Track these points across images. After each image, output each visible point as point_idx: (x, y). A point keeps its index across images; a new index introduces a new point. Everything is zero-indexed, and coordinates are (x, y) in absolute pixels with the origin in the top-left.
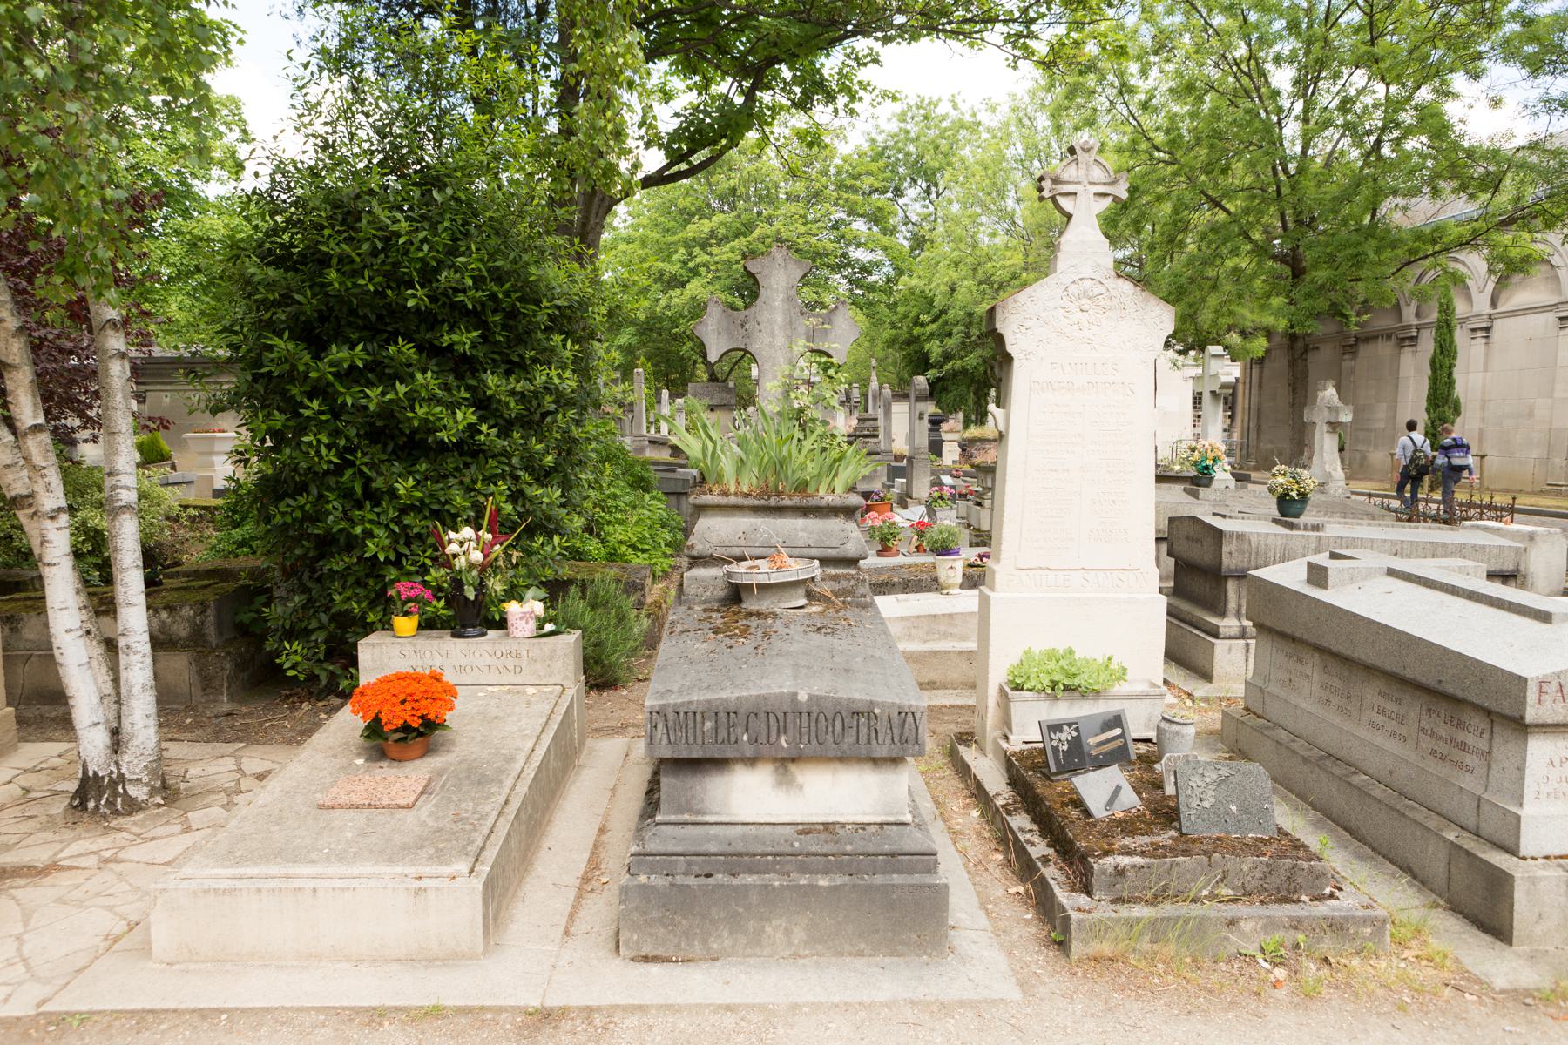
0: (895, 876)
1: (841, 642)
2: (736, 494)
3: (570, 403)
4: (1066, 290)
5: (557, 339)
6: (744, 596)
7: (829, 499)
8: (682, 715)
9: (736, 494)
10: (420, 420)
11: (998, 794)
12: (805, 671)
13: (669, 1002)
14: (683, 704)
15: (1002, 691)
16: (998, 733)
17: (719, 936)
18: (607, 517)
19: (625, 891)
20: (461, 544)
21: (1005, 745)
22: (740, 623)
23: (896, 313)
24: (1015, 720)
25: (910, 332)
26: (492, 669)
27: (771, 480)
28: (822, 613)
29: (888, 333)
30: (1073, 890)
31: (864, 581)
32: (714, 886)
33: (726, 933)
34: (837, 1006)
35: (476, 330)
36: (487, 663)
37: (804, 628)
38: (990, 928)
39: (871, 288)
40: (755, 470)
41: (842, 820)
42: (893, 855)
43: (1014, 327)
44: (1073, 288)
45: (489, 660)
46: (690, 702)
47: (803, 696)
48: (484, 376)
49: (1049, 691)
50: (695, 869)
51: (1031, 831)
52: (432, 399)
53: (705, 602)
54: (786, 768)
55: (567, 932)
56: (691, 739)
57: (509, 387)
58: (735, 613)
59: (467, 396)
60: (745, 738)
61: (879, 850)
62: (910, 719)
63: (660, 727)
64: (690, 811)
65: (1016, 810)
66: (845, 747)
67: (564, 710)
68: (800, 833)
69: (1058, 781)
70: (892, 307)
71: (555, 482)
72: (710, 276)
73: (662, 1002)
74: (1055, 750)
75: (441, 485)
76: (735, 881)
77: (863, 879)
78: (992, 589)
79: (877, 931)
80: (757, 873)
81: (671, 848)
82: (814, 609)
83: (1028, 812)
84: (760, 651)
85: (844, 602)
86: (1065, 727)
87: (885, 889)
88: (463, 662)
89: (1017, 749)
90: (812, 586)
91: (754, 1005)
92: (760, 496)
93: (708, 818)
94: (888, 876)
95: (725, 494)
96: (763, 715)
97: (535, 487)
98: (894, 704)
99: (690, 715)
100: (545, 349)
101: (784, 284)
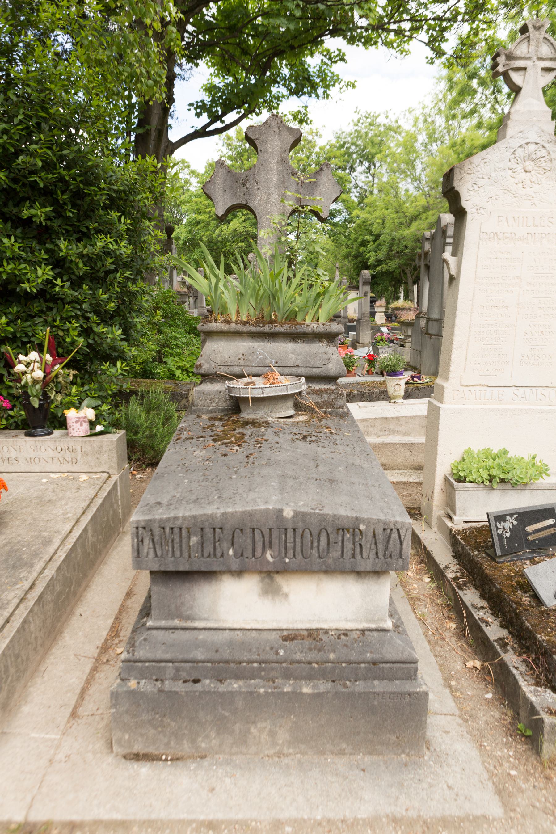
0: (376, 682)
1: (324, 450)
2: (236, 323)
3: (127, 266)
4: (514, 153)
5: (115, 215)
6: (242, 407)
7: (314, 327)
8: (168, 530)
9: (236, 323)
10: (8, 274)
11: (447, 567)
12: (290, 482)
13: (153, 816)
14: (168, 519)
15: (446, 480)
16: (441, 513)
17: (207, 737)
18: (170, 351)
19: (115, 696)
20: (28, 365)
21: (449, 524)
22: (238, 431)
23: (350, 239)
24: (458, 504)
25: (358, 251)
26: (55, 460)
27: (266, 310)
28: (307, 422)
29: (344, 251)
30: (538, 684)
31: (342, 395)
32: (200, 693)
33: (213, 734)
34: (320, 824)
35: (51, 206)
36: (51, 456)
37: (292, 436)
38: (457, 712)
39: (335, 225)
40: (253, 302)
41: (325, 626)
42: (374, 663)
43: (469, 185)
44: (520, 152)
45: (52, 454)
46: (176, 518)
47: (288, 513)
48: (58, 242)
49: (487, 483)
50: (184, 674)
51: (482, 608)
52: (15, 259)
53: (211, 412)
54: (272, 579)
55: (74, 715)
56: (178, 553)
57: (78, 251)
58: (234, 422)
59: (46, 257)
60: (231, 552)
61: (361, 658)
62: (395, 535)
63: (147, 541)
64: (181, 617)
65: (465, 584)
66: (330, 561)
67: (106, 494)
68: (285, 639)
69: (502, 562)
70: (348, 237)
71: (117, 323)
72: (244, 217)
73: (145, 817)
74: (501, 536)
75: (29, 323)
76: (222, 688)
77: (345, 686)
78: (441, 401)
79: (359, 733)
80: (243, 678)
81: (159, 655)
82: (301, 418)
83: (476, 587)
84: (251, 459)
85: (325, 412)
86: (508, 518)
87: (366, 696)
88: (33, 455)
89: (460, 529)
90: (299, 399)
91: (237, 822)
92: (256, 324)
93: (197, 624)
94: (369, 683)
95: (228, 322)
96: (249, 531)
97: (102, 325)
98: (379, 521)
99: (176, 531)
100: (107, 223)
101: (278, 148)
